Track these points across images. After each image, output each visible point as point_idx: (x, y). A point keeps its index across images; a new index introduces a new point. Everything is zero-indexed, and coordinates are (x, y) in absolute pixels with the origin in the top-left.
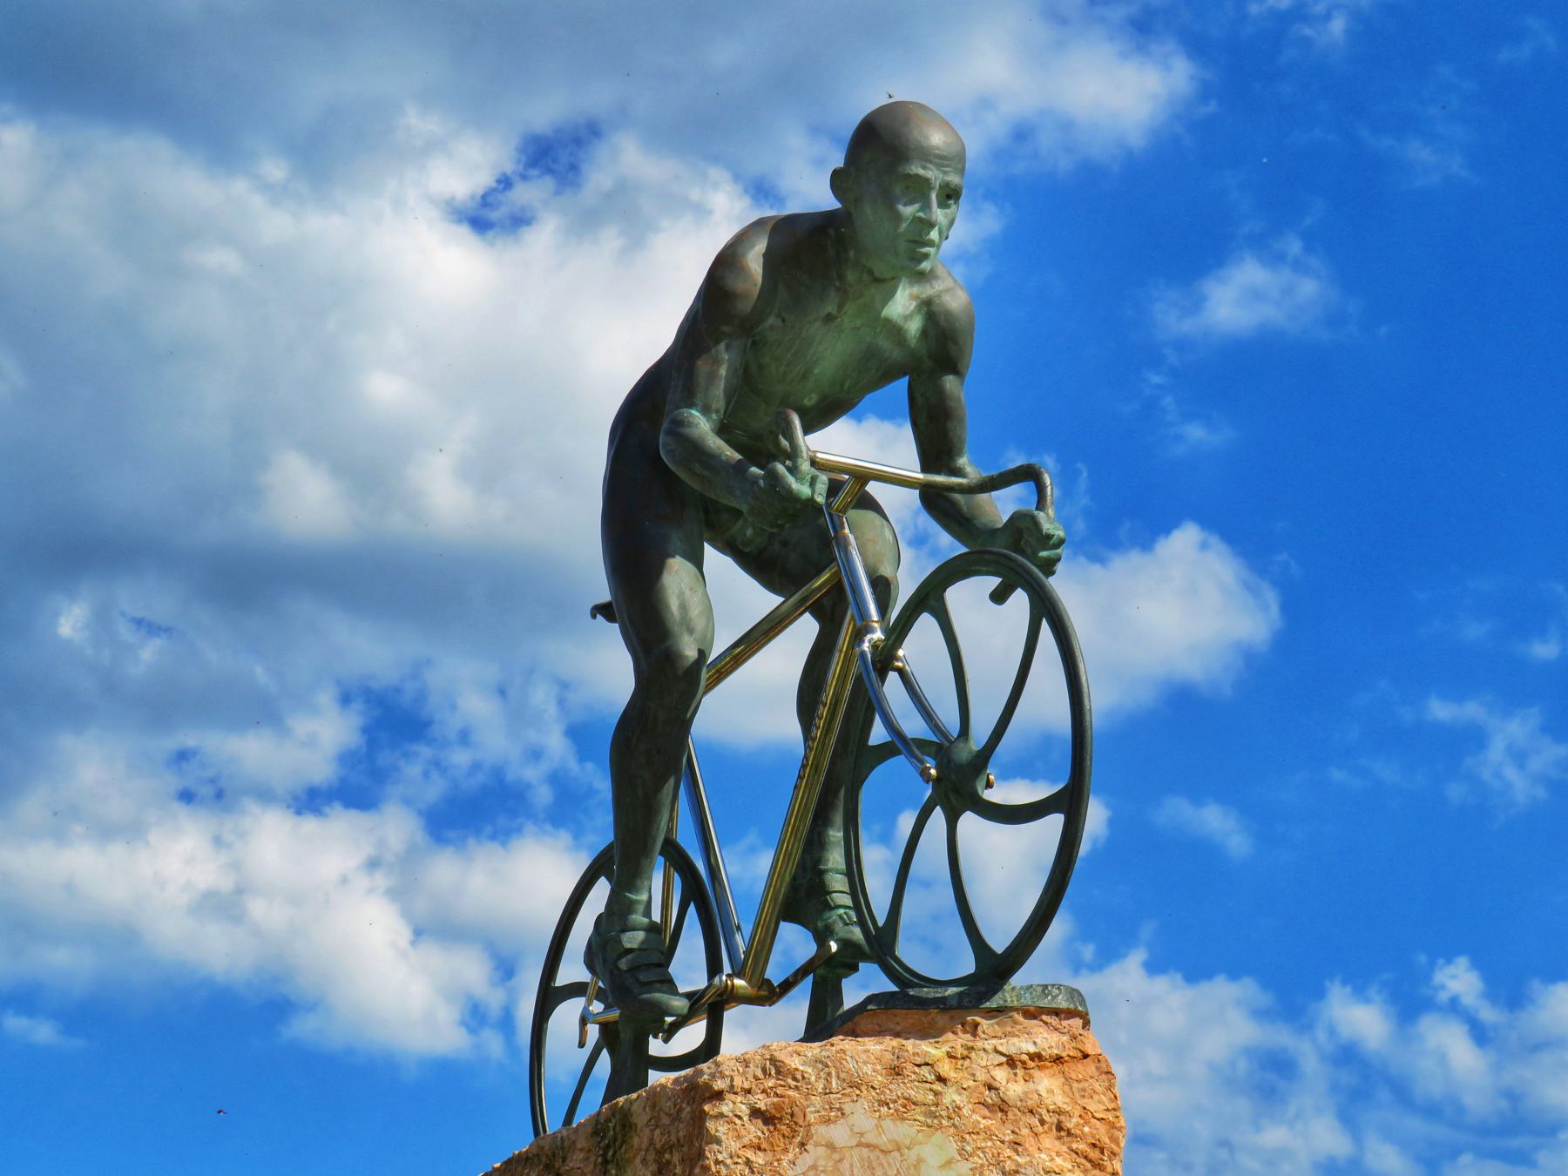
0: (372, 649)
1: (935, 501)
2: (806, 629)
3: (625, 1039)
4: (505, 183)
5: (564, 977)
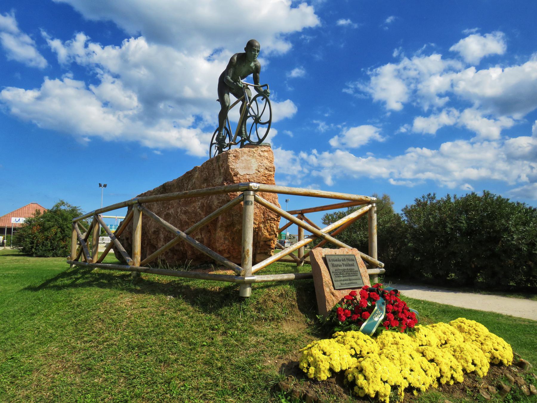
0: (196, 110)
1: (256, 89)
2: (241, 103)
3: (220, 149)
4: (212, 55)
5: (213, 142)
